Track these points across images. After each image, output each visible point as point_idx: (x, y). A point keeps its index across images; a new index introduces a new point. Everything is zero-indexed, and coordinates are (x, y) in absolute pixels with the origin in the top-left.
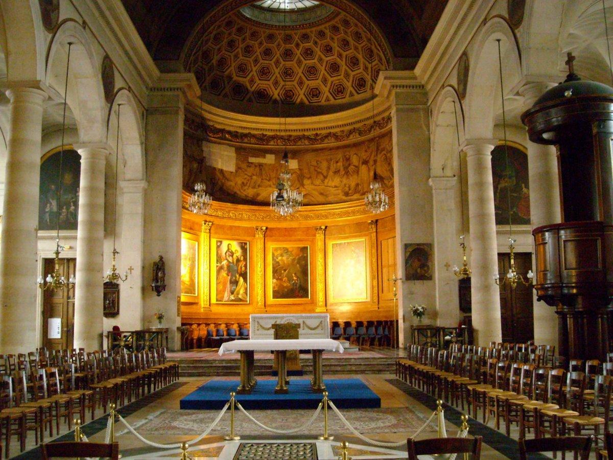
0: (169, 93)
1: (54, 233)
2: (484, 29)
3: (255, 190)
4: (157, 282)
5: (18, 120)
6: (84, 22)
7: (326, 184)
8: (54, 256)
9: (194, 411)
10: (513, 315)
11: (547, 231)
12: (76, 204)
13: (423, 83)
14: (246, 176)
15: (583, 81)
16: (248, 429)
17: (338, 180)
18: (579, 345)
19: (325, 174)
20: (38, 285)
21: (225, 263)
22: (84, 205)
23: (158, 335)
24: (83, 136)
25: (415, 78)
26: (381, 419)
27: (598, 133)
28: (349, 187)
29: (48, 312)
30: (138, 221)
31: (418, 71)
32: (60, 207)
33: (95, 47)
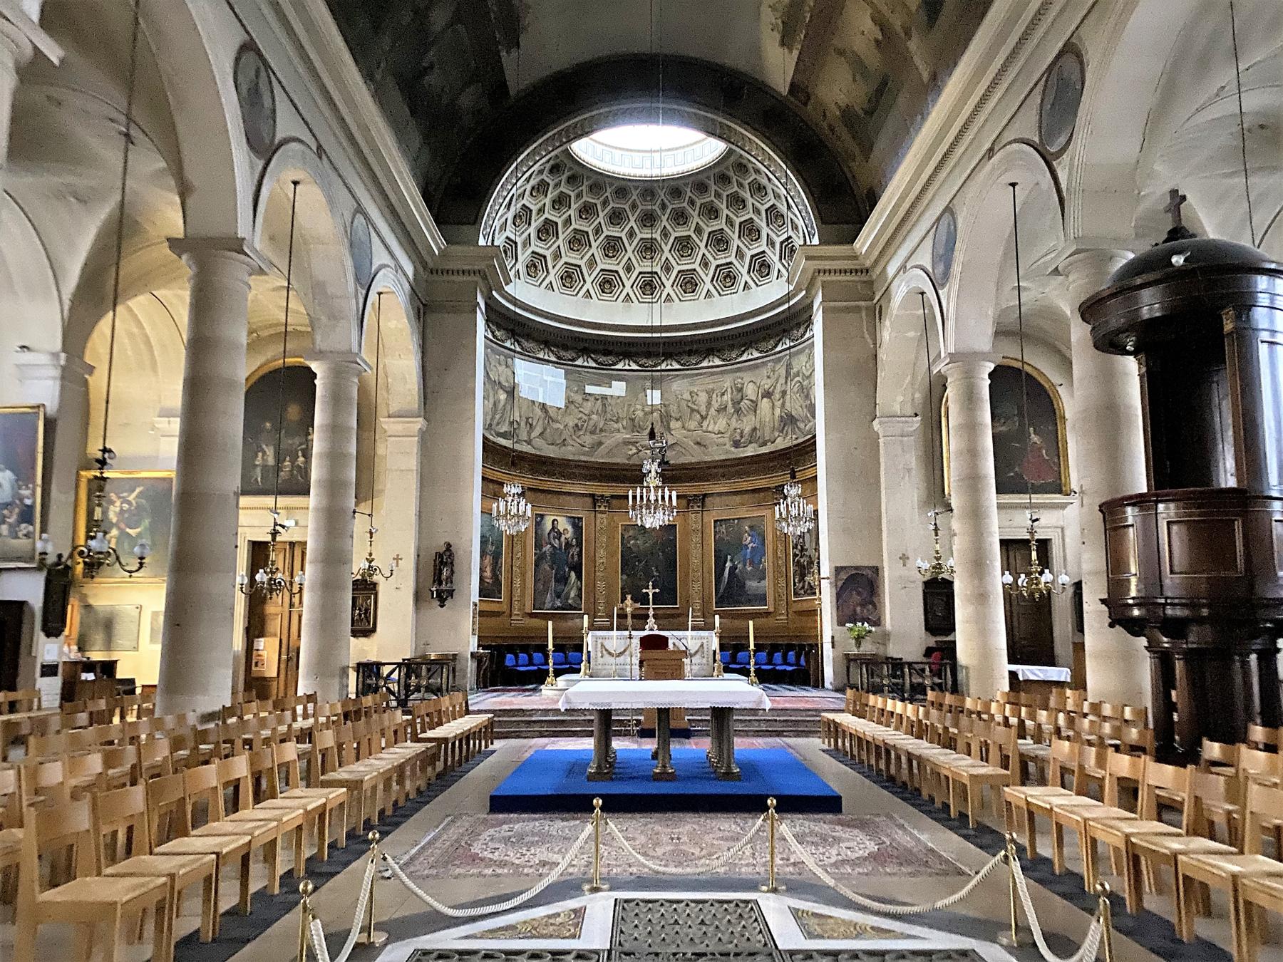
0: (461, 278)
3: (595, 437)
4: (440, 583)
6: (319, 146)
8: (269, 538)
11: (1133, 505)
12: (307, 454)
13: (868, 264)
18: (1195, 717)
19: (704, 413)
20: (238, 587)
21: (547, 548)
22: (321, 455)
28: (742, 432)
30: (412, 483)
31: (857, 244)
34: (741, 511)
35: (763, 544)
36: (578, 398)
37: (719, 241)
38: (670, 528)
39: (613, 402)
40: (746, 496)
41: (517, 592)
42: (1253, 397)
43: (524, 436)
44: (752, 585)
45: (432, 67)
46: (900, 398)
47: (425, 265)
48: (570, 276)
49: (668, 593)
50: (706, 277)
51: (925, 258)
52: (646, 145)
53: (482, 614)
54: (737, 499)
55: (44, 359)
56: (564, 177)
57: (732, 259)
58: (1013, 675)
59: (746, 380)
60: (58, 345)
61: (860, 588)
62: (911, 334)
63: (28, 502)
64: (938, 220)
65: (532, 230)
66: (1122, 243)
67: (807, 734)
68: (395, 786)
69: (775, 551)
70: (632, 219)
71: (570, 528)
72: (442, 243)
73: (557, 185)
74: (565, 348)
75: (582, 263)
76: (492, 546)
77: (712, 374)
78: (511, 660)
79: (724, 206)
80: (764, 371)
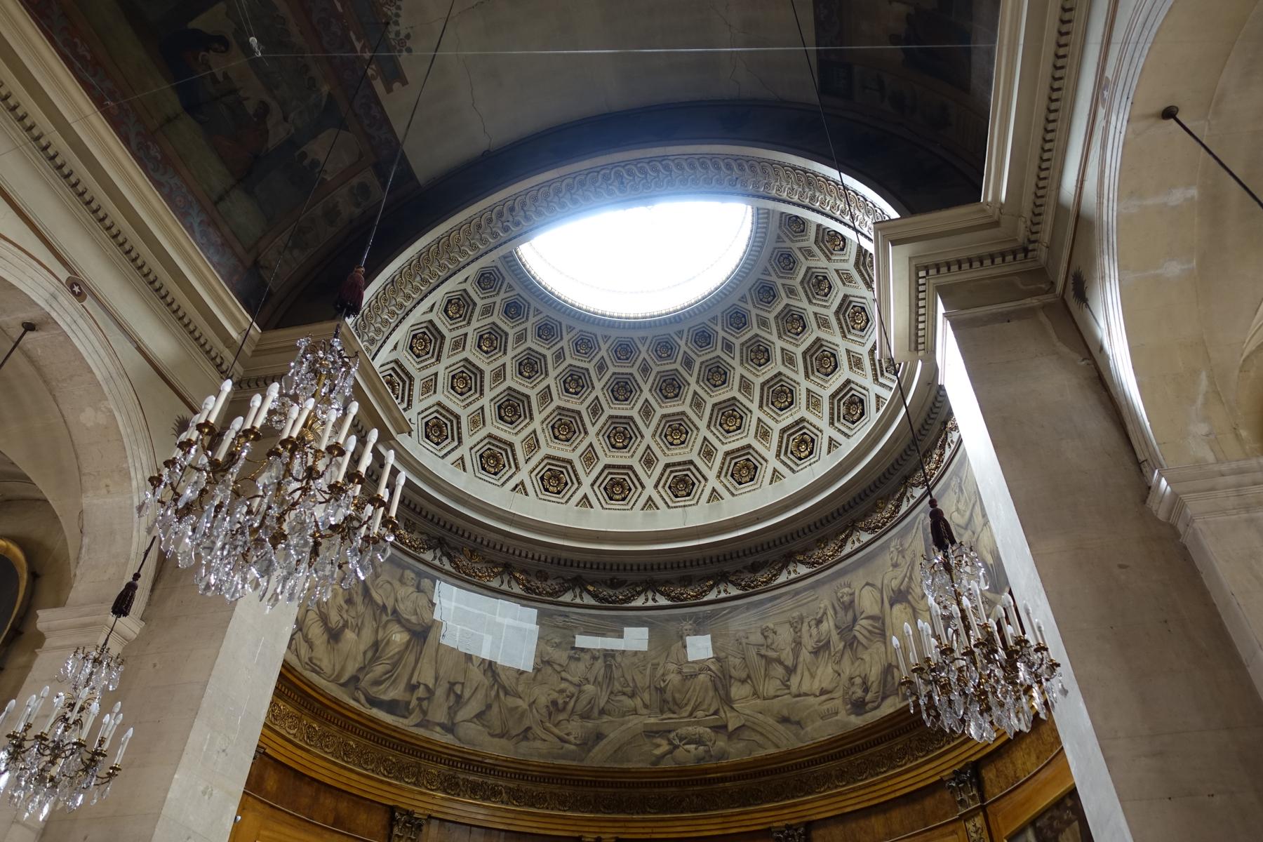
3: (590, 724)
7: (794, 689)
14: (564, 685)
17: (830, 670)
19: (789, 663)
31: (987, 195)
40: (896, 815)
43: (440, 715)
46: (1203, 428)
48: (556, 476)
59: (857, 585)
70: (646, 388)
74: (543, 576)
77: (797, 593)
80: (887, 558)
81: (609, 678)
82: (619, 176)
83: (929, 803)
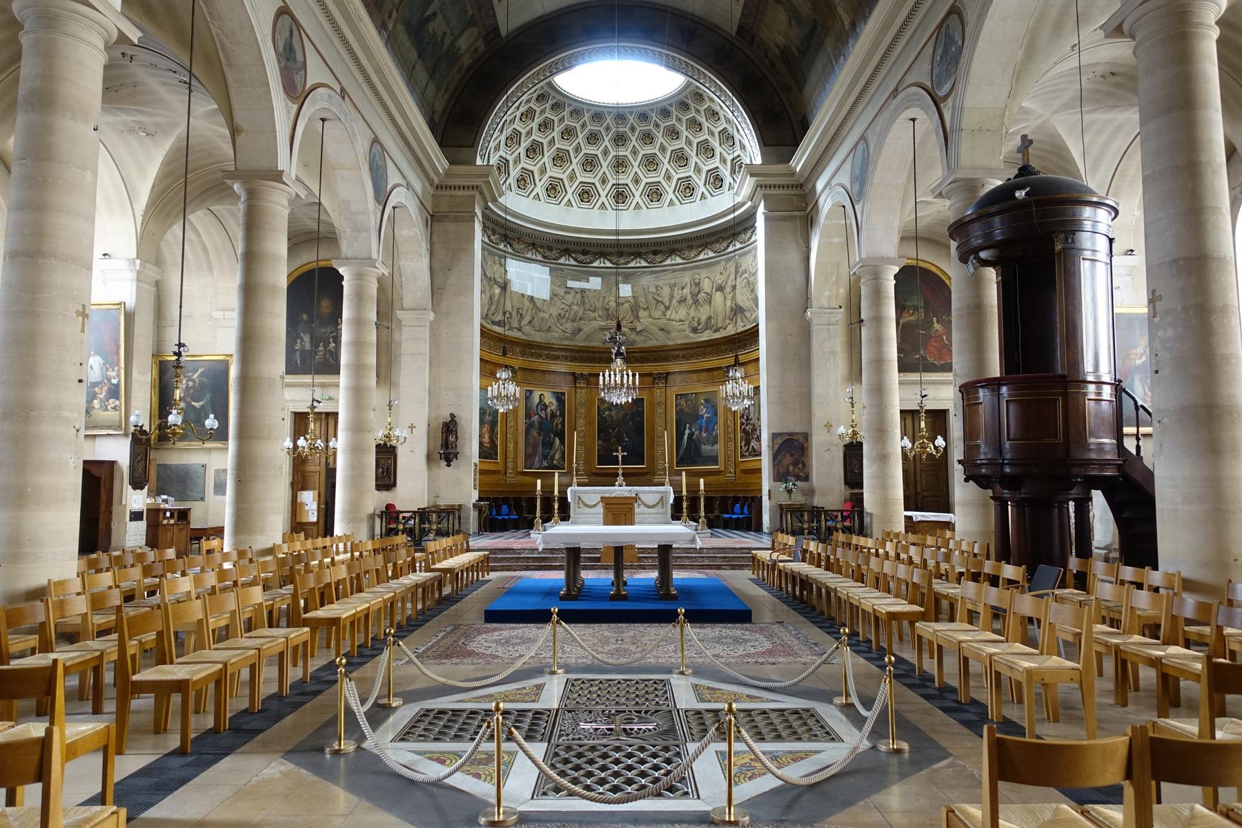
0: (461, 193)
1: (307, 379)
2: (895, 103)
5: (253, 225)
6: (342, 89)
9: (495, 625)
10: (916, 493)
11: (982, 387)
12: (337, 340)
15: (1042, 175)
16: (573, 655)
23: (448, 513)
24: (346, 248)
25: (793, 174)
26: (748, 641)
27: (1064, 249)
29: (299, 482)
31: (792, 163)
32: (315, 342)
33: (359, 127)
34: (699, 387)
35: (716, 414)
36: (561, 291)
37: (680, 158)
38: (638, 402)
39: (591, 295)
40: (703, 375)
41: (511, 455)
42: (1074, 307)
44: (706, 448)
45: (435, 14)
46: (827, 294)
47: (431, 182)
49: (635, 455)
50: (669, 189)
51: (844, 178)
52: (618, 77)
53: (482, 472)
54: (694, 376)
55: (124, 264)
56: (548, 105)
57: (691, 173)
58: (908, 518)
60: (133, 253)
61: (793, 452)
62: (836, 240)
63: (114, 381)
64: (855, 146)
65: (522, 150)
66: (991, 172)
67: (741, 567)
68: (409, 605)
69: (726, 421)
71: (554, 401)
72: (446, 163)
73: (543, 112)
74: (550, 249)
75: (564, 177)
76: (489, 418)
77: (674, 271)
78: (508, 508)
79: (684, 129)
80: (719, 268)
81: (583, 303)
82: (619, 51)
83: (716, 373)
